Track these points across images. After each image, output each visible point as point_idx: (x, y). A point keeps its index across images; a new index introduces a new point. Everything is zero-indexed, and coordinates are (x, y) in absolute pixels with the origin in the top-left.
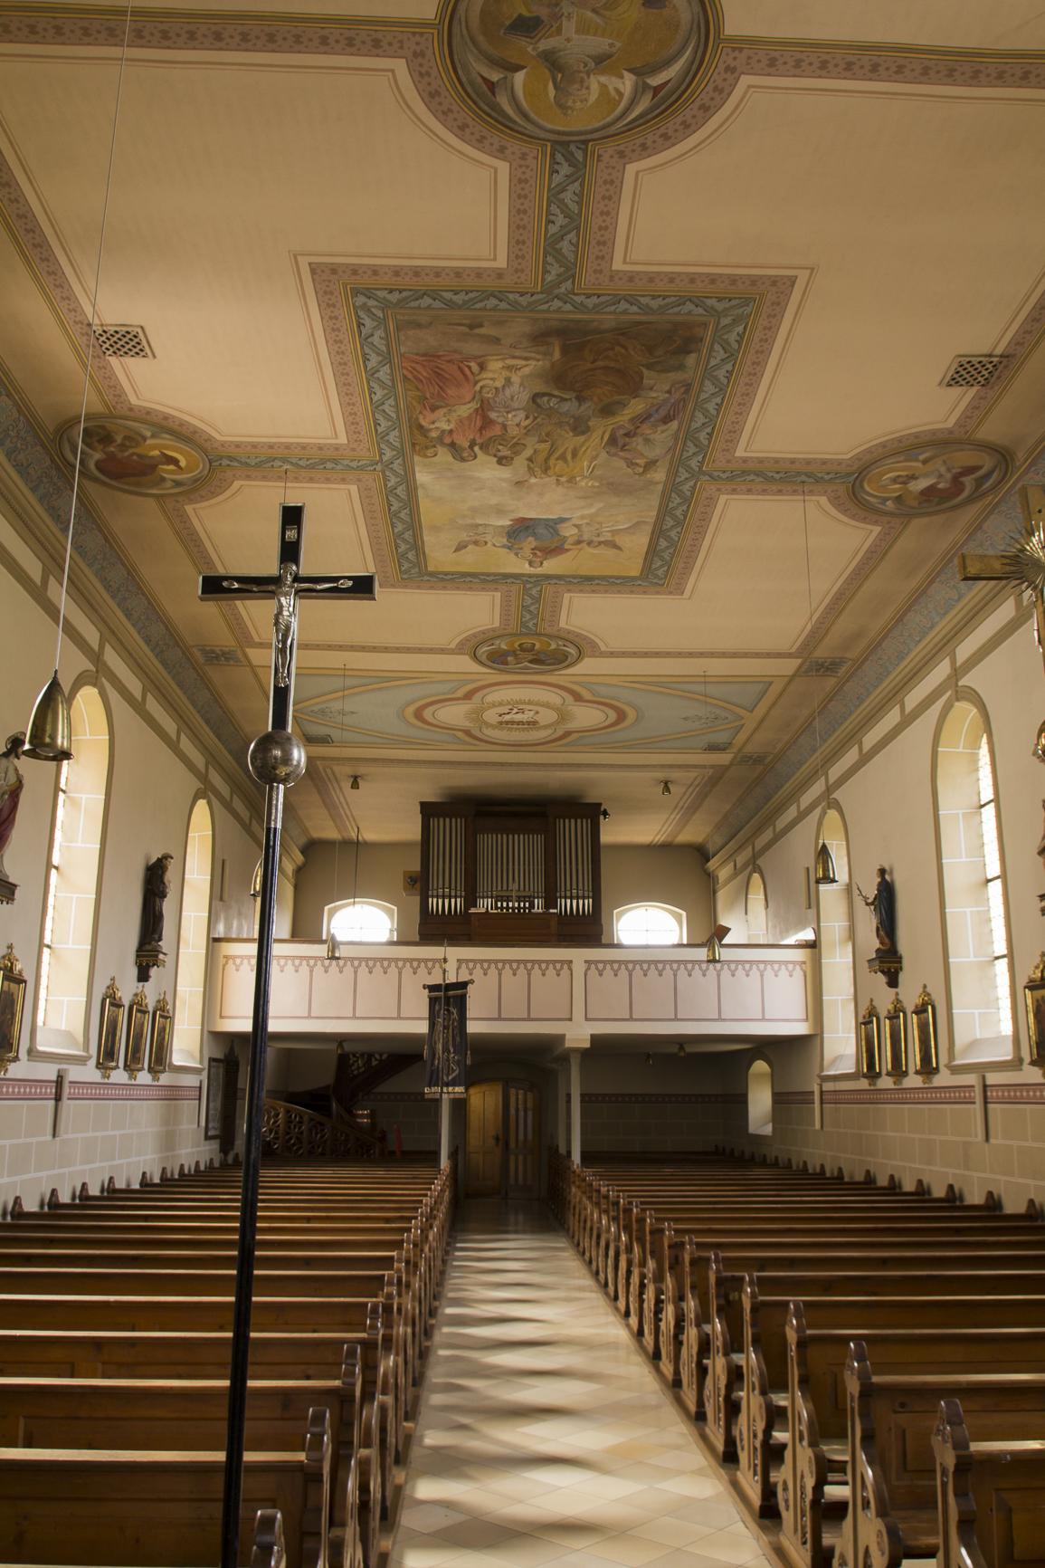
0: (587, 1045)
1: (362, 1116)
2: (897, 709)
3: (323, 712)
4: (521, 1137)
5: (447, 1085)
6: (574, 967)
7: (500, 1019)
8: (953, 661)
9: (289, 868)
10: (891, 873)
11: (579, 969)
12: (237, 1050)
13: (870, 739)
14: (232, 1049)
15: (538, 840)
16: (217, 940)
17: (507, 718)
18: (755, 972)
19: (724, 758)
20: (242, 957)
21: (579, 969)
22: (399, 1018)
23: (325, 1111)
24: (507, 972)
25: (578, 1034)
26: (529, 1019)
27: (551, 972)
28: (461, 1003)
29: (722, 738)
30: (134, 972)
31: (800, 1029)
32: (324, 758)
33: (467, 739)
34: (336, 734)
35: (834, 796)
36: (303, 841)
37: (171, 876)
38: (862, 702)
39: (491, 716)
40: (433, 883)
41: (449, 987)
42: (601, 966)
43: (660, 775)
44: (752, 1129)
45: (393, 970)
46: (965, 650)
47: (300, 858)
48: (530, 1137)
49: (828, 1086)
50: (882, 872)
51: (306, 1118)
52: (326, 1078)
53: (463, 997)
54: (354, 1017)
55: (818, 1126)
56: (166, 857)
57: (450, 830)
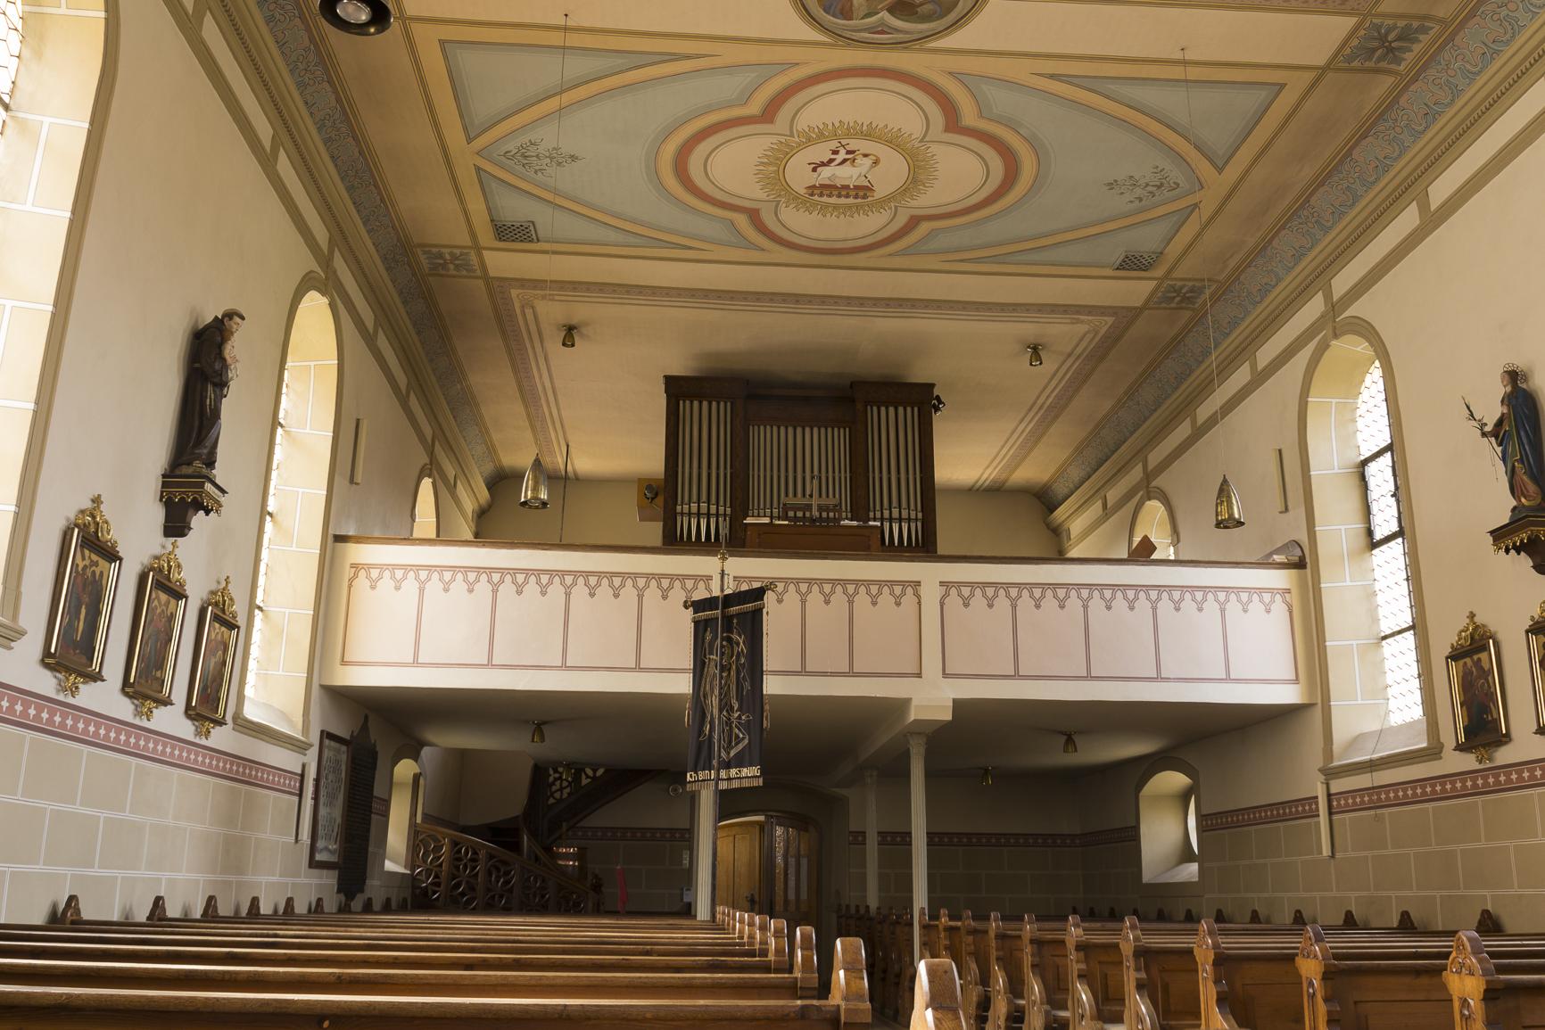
0: (949, 717)
1: (567, 857)
2: (1188, 422)
3: (523, 155)
4: (792, 896)
5: (728, 766)
6: (923, 591)
7: (803, 672)
8: (1254, 366)
9: (469, 506)
10: (1525, 378)
11: (931, 594)
12: (374, 735)
13: (1440, 190)
14: (365, 728)
15: (838, 439)
16: (340, 539)
17: (826, 174)
18: (1211, 606)
19: (1136, 291)
20: (382, 567)
21: (931, 594)
22: (638, 668)
23: (515, 847)
24: (815, 598)
25: (932, 699)
26: (851, 673)
27: (886, 598)
28: (753, 625)
29: (1145, 240)
30: (158, 514)
31: (1287, 695)
32: (523, 283)
33: (752, 234)
34: (544, 219)
35: (1154, 484)
36: (489, 468)
37: (240, 349)
38: (1386, 170)
39: (799, 175)
40: (682, 491)
41: (729, 600)
42: (966, 591)
43: (1028, 329)
44: (1148, 876)
45: (629, 592)
46: (1155, 458)
47: (484, 495)
48: (804, 896)
49: (1338, 786)
50: (1513, 376)
51: (482, 854)
52: (512, 804)
53: (757, 615)
54: (565, 667)
55: (1326, 851)
56: (230, 315)
57: (709, 420)
